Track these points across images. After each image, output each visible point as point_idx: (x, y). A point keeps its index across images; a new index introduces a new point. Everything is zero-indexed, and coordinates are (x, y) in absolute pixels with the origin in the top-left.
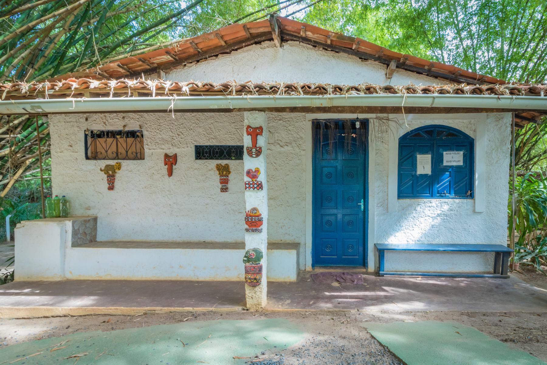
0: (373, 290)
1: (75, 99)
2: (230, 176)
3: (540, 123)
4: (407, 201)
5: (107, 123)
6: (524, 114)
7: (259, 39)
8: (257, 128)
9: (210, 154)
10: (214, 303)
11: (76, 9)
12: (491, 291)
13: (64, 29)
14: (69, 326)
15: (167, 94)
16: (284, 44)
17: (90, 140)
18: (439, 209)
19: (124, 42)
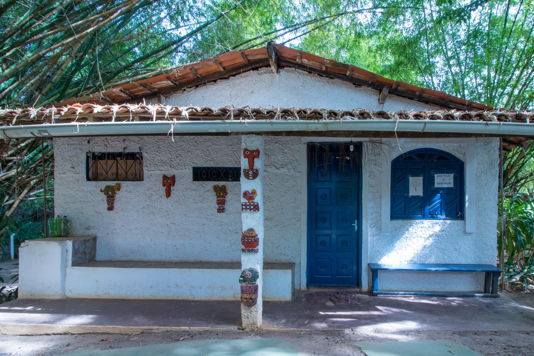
0: (367, 310)
1: (80, 123)
2: (226, 197)
3: (526, 147)
4: (400, 222)
5: (108, 145)
6: (511, 139)
7: (257, 65)
9: (207, 175)
10: (210, 323)
11: (83, 38)
12: (481, 310)
13: (71, 56)
14: (69, 344)
15: (167, 118)
16: (280, 70)
17: (91, 162)
18: (430, 230)
19: (127, 68)
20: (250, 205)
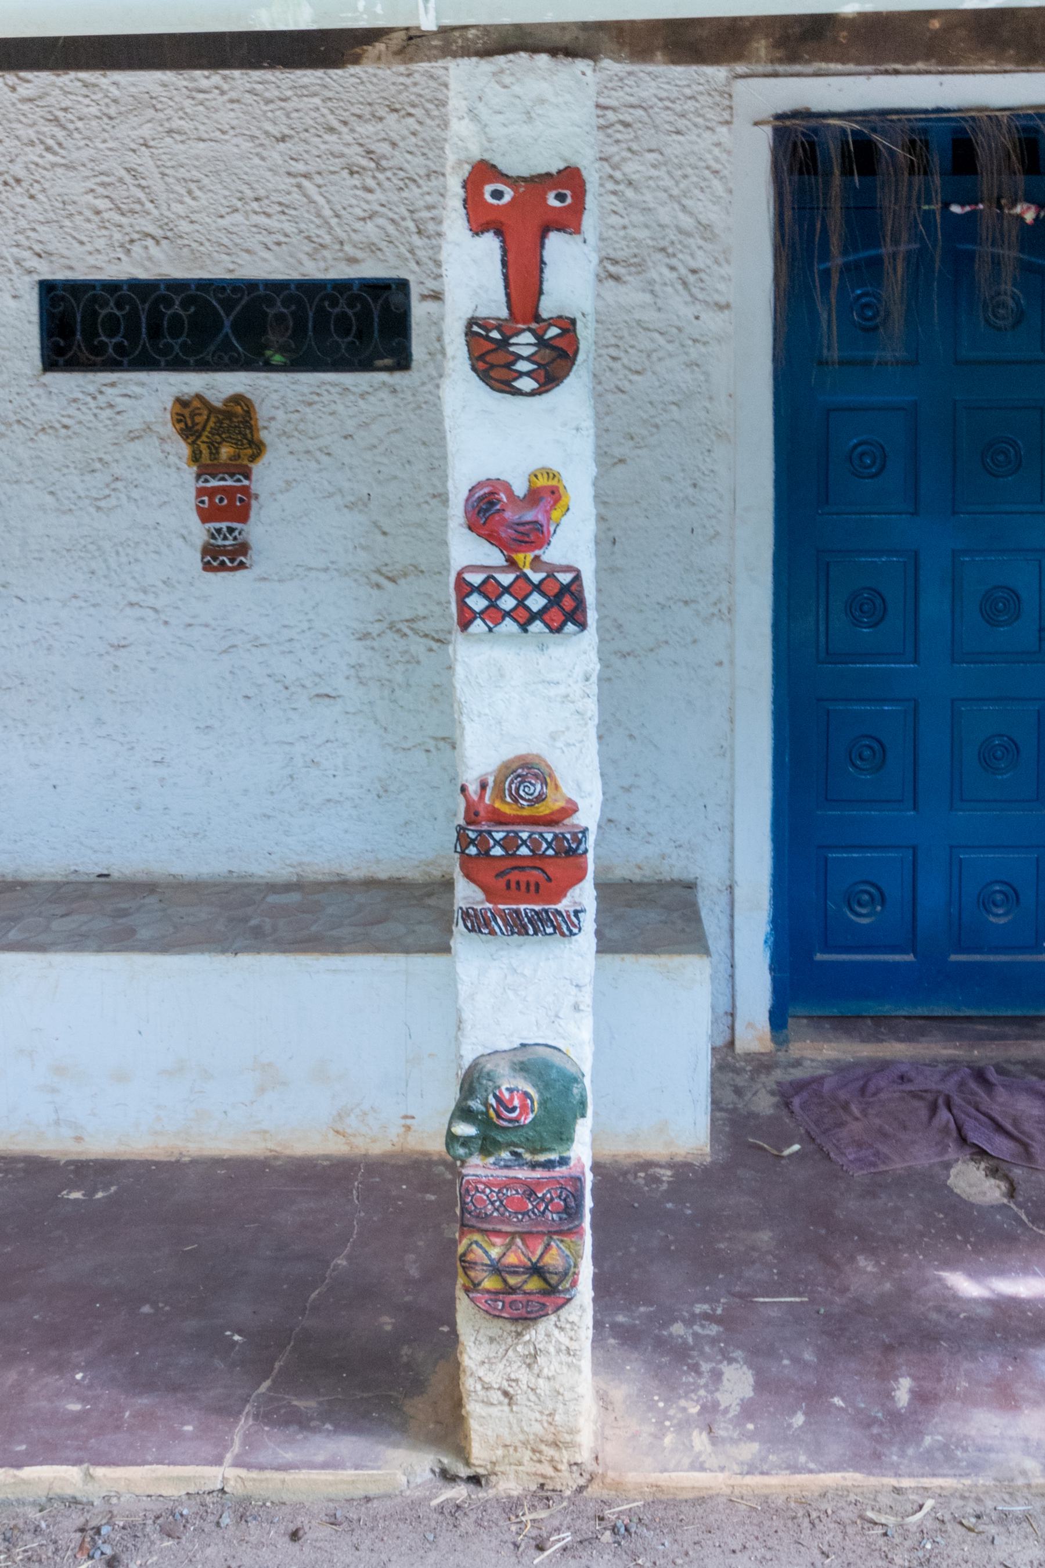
2: (258, 469)
8: (542, 181)
9: (133, 333)
10: (228, 1411)
20: (522, 588)
